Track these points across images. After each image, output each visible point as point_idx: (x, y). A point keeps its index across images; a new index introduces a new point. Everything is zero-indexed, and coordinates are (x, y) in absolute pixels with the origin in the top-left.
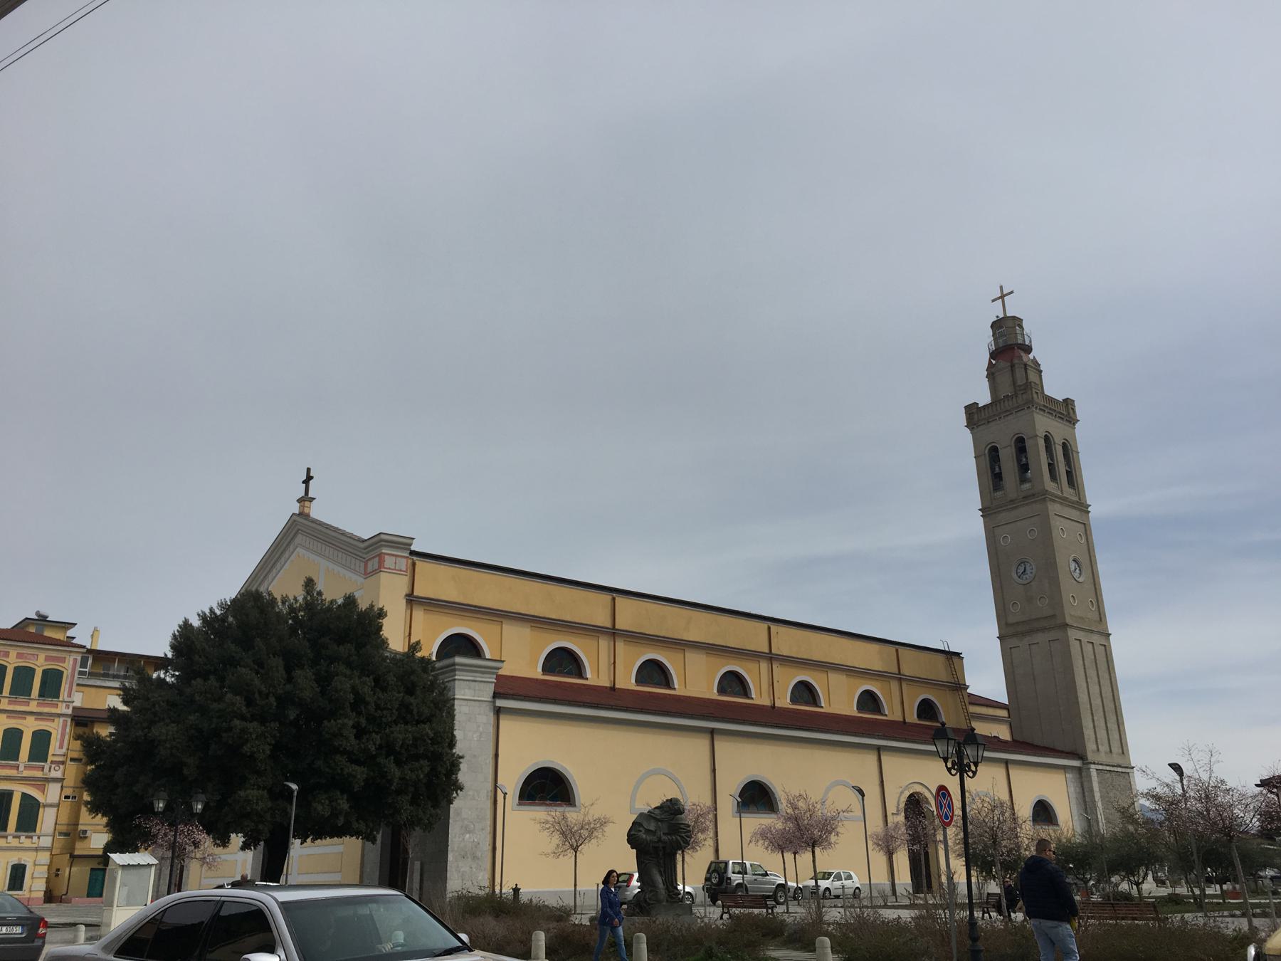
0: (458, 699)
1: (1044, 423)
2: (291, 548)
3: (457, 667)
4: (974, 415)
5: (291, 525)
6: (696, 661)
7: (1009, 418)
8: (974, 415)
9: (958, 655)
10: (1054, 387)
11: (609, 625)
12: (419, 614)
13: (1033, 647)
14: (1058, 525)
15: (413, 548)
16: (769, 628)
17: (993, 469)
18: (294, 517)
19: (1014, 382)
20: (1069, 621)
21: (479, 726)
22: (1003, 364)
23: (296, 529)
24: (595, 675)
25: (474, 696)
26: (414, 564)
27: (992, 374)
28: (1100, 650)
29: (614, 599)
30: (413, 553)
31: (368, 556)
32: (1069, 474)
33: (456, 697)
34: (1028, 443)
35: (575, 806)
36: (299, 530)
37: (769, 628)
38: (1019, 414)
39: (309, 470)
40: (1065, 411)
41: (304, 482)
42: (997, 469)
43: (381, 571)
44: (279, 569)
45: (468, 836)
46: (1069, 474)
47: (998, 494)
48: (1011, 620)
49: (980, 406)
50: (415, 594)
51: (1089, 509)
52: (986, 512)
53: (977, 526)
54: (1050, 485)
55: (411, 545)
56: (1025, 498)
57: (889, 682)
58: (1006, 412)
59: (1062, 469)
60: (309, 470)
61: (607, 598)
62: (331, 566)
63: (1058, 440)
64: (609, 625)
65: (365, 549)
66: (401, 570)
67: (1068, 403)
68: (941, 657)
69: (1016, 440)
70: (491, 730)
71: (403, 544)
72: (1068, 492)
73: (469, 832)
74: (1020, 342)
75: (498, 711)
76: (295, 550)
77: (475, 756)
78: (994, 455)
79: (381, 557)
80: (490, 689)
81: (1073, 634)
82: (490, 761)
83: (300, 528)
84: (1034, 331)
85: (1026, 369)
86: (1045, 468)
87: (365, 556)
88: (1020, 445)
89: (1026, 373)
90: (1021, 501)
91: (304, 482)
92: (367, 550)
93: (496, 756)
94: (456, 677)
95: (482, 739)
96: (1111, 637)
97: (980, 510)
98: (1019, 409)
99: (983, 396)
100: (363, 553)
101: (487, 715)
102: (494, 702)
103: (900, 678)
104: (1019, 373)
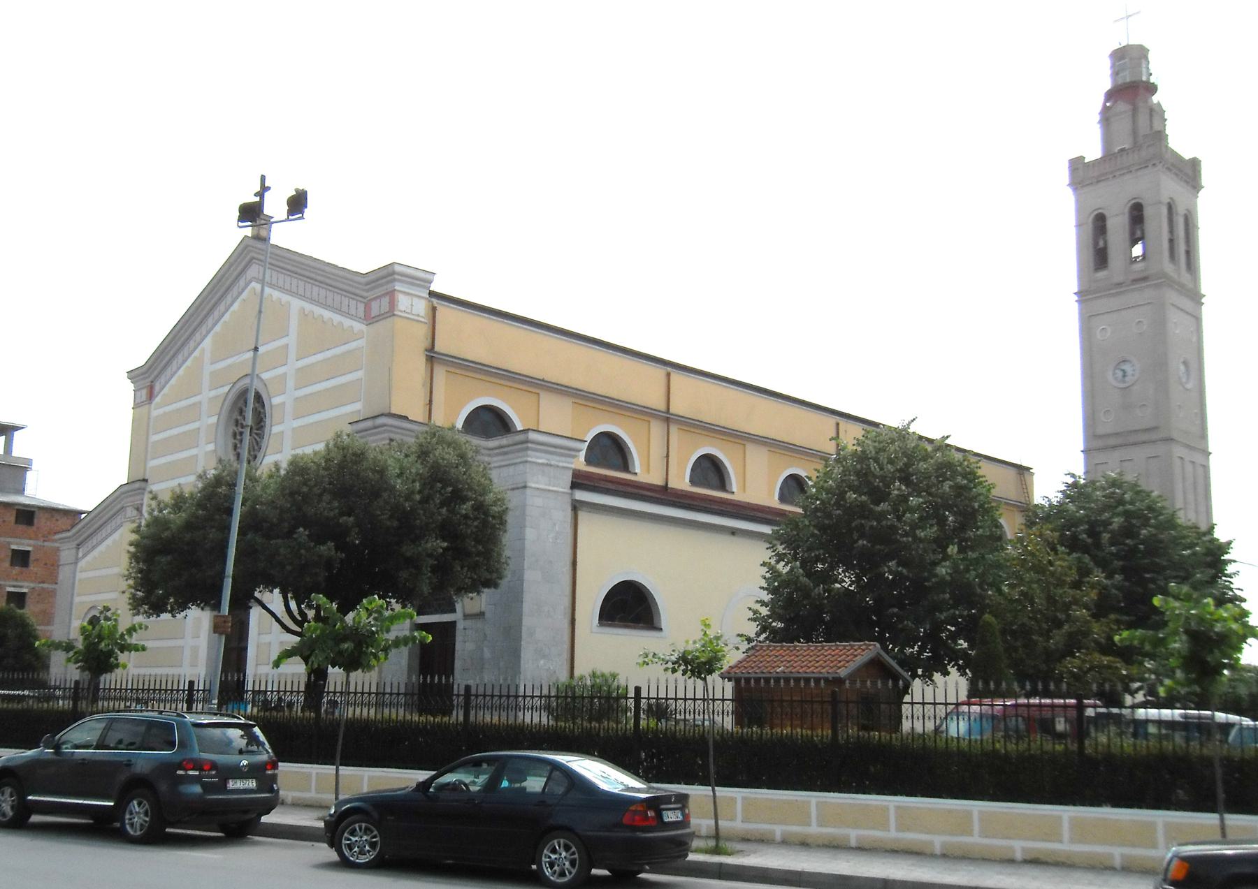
0: (530, 487)
1: (1170, 187)
2: (242, 283)
3: (530, 445)
4: (1081, 173)
5: (243, 251)
6: (757, 459)
7: (1128, 176)
8: (1081, 173)
9: (1028, 469)
10: (1180, 141)
11: (662, 407)
12: (440, 373)
13: (1125, 464)
14: (1174, 317)
15: (436, 287)
16: (838, 424)
17: (1096, 243)
18: (247, 239)
19: (1135, 132)
20: (1175, 435)
21: (555, 524)
22: (1122, 107)
23: (248, 257)
24: (645, 470)
25: (549, 485)
26: (434, 309)
27: (1107, 117)
28: (1200, 471)
29: (668, 375)
30: (432, 294)
31: (370, 295)
32: (1188, 253)
33: (529, 484)
34: (1148, 212)
35: (661, 629)
36: (254, 258)
37: (838, 424)
38: (1140, 173)
39: (263, 178)
40: (1190, 172)
41: (269, 188)
42: (1101, 244)
43: (394, 315)
44: (216, 317)
45: (542, 662)
46: (1189, 253)
47: (1102, 274)
48: (1101, 430)
49: (1086, 161)
50: (437, 349)
51: (1203, 300)
52: (1085, 295)
53: (1070, 312)
54: (1168, 267)
55: (430, 282)
56: (1135, 281)
57: (649, 422)
58: (1122, 169)
59: (1181, 248)
60: (263, 178)
61: (660, 372)
62: (308, 307)
63: (1181, 209)
64: (662, 407)
65: (367, 284)
66: (418, 315)
67: (1195, 164)
68: (1013, 471)
69: (1097, 215)
70: (568, 530)
71: (420, 280)
72: (1185, 277)
73: (544, 657)
74: (1144, 79)
75: (576, 506)
76: (247, 285)
77: (551, 562)
78: (1099, 224)
79: (391, 294)
80: (568, 478)
81: (1178, 451)
82: (567, 568)
83: (256, 256)
84: (1158, 71)
85: (1151, 115)
86: (1166, 245)
87: (365, 294)
88: (1135, 213)
89: (1151, 121)
90: (1130, 285)
91: (269, 188)
92: (369, 286)
93: (574, 563)
94: (529, 459)
95: (558, 541)
96: (1211, 457)
97: (1075, 293)
98: (1144, 165)
99: (1093, 151)
100: (364, 290)
101: (563, 511)
102: (572, 494)
103: (668, 418)
104: (1143, 120)
